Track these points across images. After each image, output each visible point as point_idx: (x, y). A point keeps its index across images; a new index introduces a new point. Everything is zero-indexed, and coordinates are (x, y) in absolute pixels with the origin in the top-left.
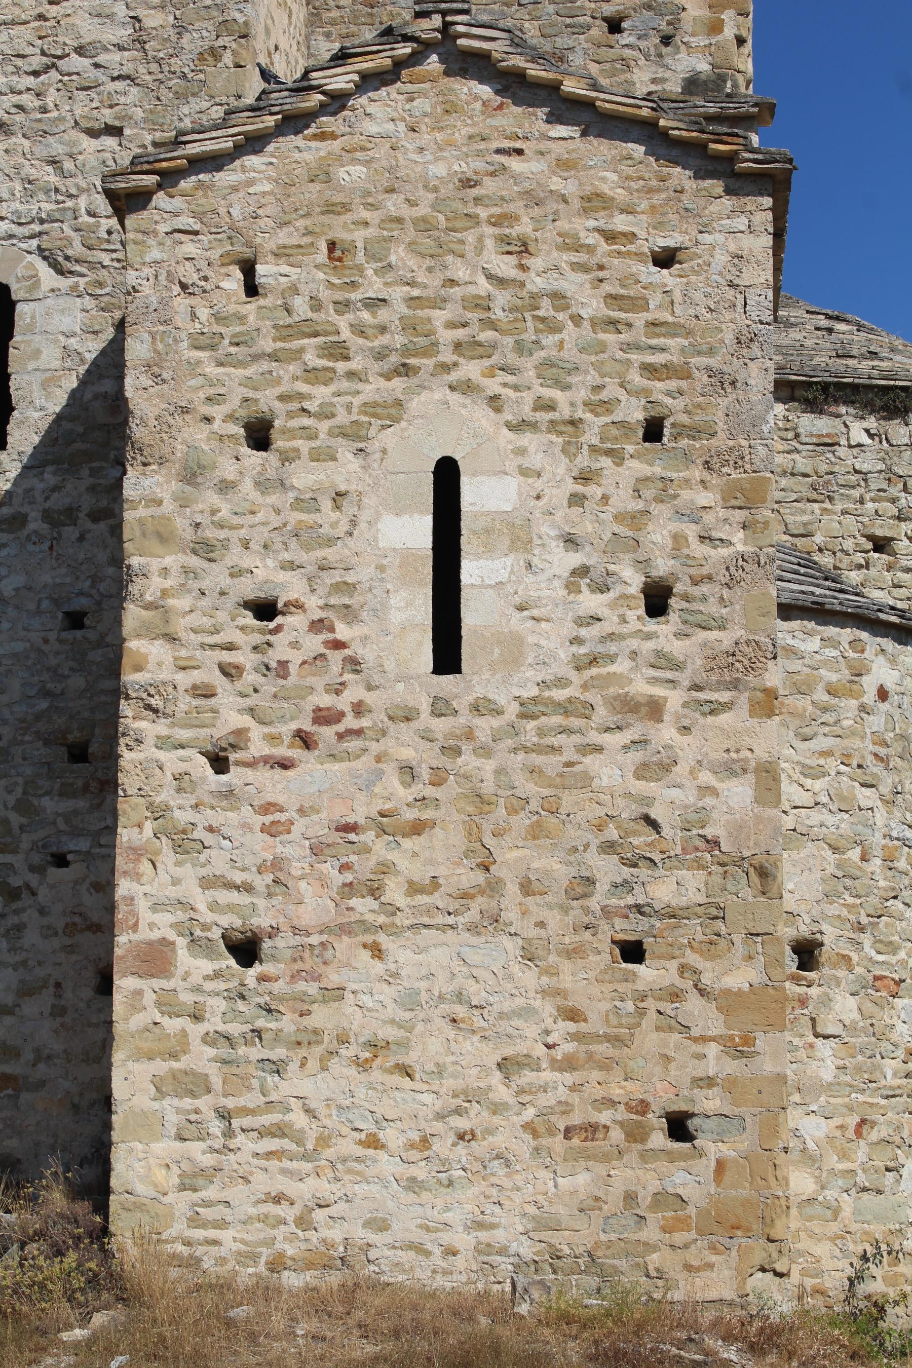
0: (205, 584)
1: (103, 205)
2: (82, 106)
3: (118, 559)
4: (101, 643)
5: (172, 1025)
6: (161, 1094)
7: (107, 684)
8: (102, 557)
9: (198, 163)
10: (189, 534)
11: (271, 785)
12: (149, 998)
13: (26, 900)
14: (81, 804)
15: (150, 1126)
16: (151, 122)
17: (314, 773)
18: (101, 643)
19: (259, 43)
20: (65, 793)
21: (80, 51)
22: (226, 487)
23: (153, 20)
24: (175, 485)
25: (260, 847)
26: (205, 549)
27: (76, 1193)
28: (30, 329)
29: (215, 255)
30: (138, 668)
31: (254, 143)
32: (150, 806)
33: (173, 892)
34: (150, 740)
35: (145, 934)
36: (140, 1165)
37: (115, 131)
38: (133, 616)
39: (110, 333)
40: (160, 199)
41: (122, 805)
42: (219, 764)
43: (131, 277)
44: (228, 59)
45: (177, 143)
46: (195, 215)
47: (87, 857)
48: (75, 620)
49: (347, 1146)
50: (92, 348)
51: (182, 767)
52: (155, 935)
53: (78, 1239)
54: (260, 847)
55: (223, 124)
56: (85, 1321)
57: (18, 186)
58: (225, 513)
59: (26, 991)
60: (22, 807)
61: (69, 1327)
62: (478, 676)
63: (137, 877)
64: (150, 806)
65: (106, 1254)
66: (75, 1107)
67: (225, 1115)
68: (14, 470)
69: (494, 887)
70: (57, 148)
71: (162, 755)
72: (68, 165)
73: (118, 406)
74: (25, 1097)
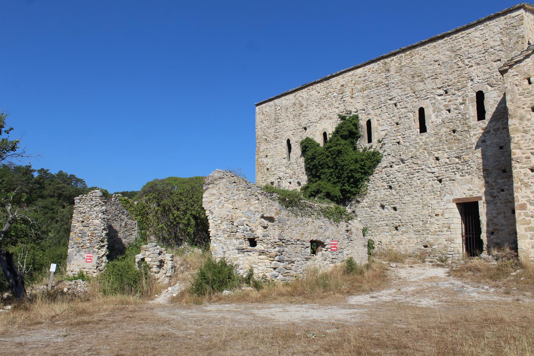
0: (526, 138)
1: (499, 74)
2: (493, 57)
3: (508, 136)
4: (507, 151)
5: (527, 219)
6: (526, 231)
7: (509, 158)
8: (505, 136)
9: (516, 63)
10: (522, 129)
12: (522, 214)
13: (497, 198)
14: (506, 180)
15: (525, 237)
16: (506, 57)
18: (507, 151)
19: (526, 38)
20: (502, 178)
21: (491, 48)
22: (528, 120)
24: (518, 121)
26: (526, 132)
27: (511, 249)
28: (487, 98)
29: (522, 78)
30: (514, 155)
31: (527, 56)
32: (519, 179)
33: (525, 194)
34: (518, 167)
35: (520, 202)
36: (523, 244)
37: (499, 60)
38: (512, 145)
39: (502, 96)
40: (510, 70)
41: (514, 180)
43: (506, 85)
44: (520, 42)
45: (512, 60)
46: (517, 72)
47: (508, 189)
48: (501, 148)
50: (499, 99)
51: (525, 172)
52: (523, 202)
53: (512, 257)
55: (521, 54)
56: (515, 271)
57: (482, 73)
58: (529, 124)
59: (499, 214)
60: (494, 181)
61: (512, 272)
63: (518, 192)
64: (519, 179)
65: (518, 260)
66: (510, 234)
68: (487, 123)
70: (489, 65)
71: (521, 170)
72: (491, 68)
73: (506, 109)
74: (500, 232)
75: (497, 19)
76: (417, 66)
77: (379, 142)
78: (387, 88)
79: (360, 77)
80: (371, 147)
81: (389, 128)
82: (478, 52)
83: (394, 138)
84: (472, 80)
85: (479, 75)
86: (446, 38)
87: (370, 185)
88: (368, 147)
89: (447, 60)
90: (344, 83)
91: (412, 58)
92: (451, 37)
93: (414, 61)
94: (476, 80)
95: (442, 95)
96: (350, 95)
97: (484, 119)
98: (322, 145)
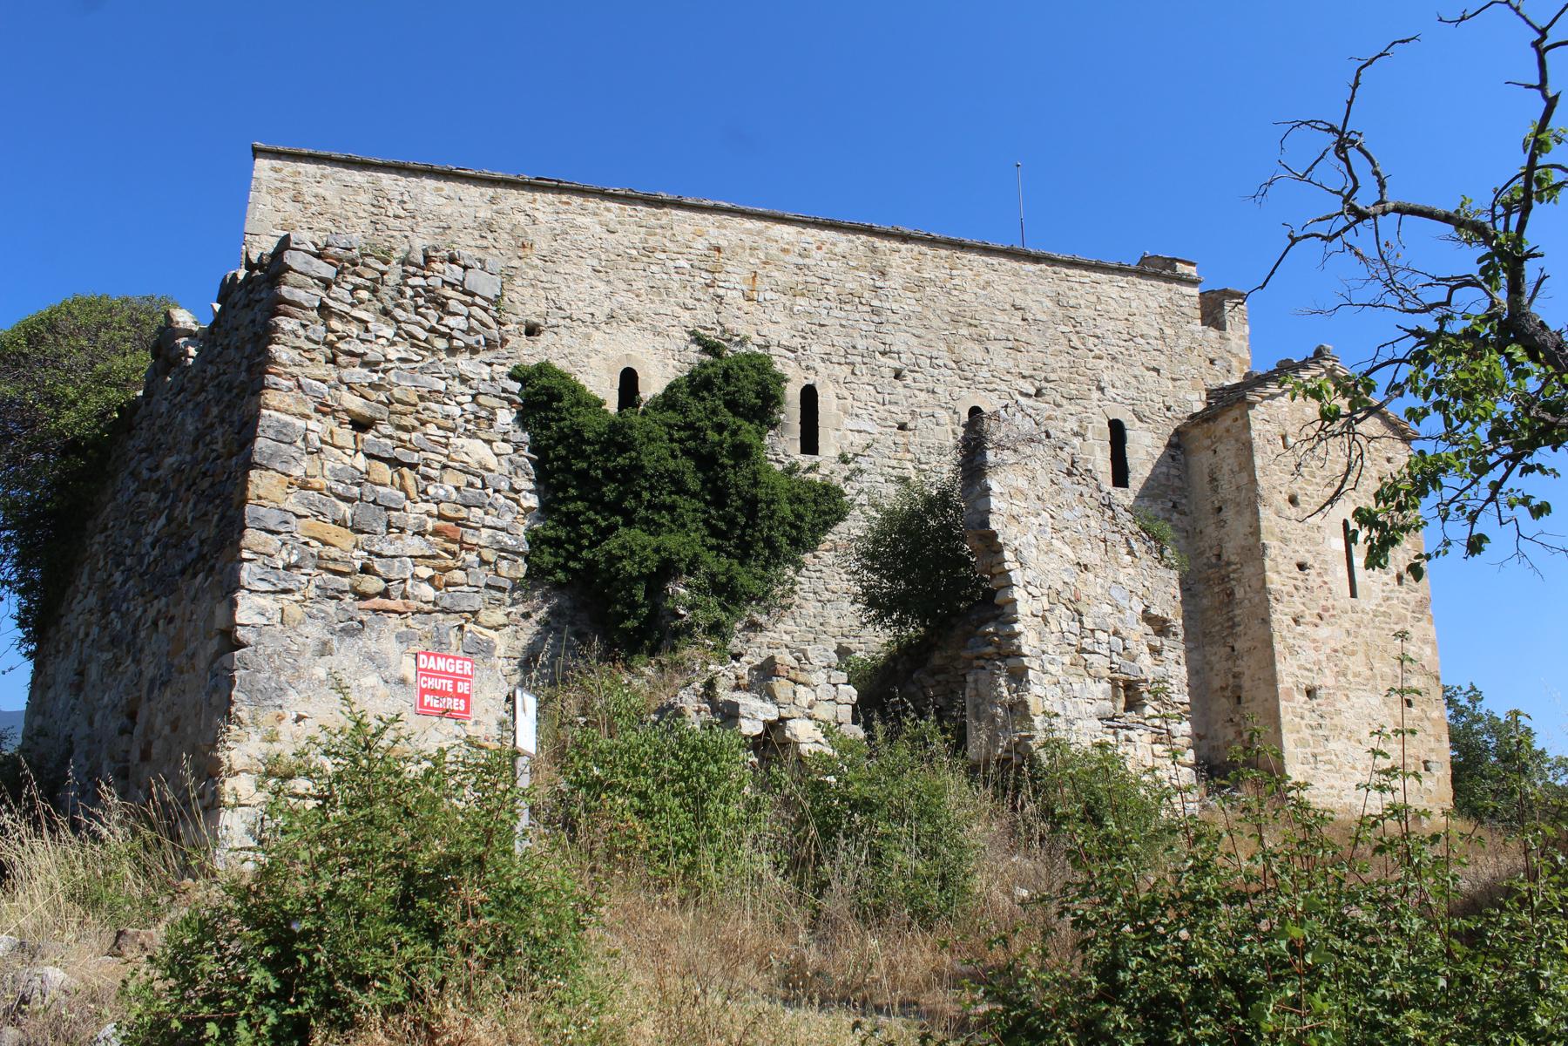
11: (1309, 630)
17: (1324, 631)
23: (1168, 331)
25: (1313, 656)
38: (1268, 563)
42: (1296, 621)
49: (1347, 769)
54: (1313, 656)
62: (1361, 601)
67: (1314, 756)
69: (1374, 676)
70: (1137, 373)
75: (1155, 283)
76: (966, 297)
77: (844, 459)
78: (876, 319)
79: (784, 250)
80: (813, 468)
81: (876, 430)
82: (1114, 333)
83: (894, 463)
84: (1101, 389)
85: (1118, 384)
86: (1043, 266)
87: (804, 582)
88: (805, 466)
89: (1044, 318)
90: (723, 243)
91: (954, 272)
92: (1057, 269)
93: (956, 281)
94: (1110, 392)
95: (1028, 395)
96: (745, 287)
97: (1126, 486)
98: (612, 406)
